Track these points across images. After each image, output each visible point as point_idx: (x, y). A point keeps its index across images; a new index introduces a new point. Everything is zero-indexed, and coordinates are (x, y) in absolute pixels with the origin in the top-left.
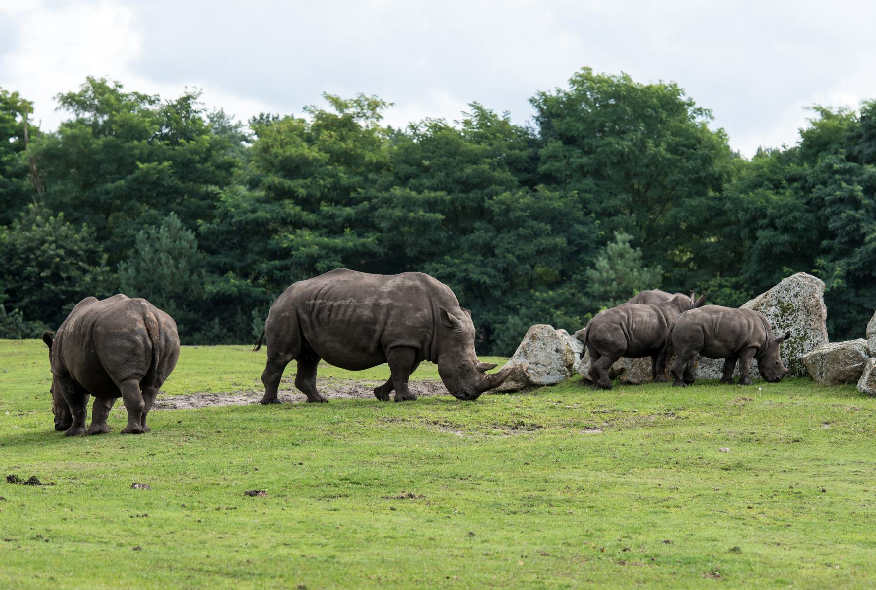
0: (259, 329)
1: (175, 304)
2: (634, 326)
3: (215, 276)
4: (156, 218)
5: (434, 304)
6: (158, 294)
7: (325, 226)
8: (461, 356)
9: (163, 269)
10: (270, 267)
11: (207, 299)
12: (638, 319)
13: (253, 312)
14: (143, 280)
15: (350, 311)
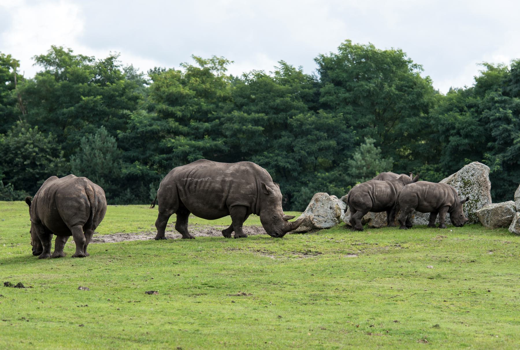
0: (154, 195)
1: (104, 180)
2: (376, 193)
3: (128, 164)
4: (92, 130)
5: (257, 180)
6: (94, 175)
7: (193, 134)
8: (274, 211)
9: (97, 160)
10: (160, 159)
11: (123, 177)
12: (378, 189)
13: (150, 185)
14: (85, 166)
15: (208, 184)
